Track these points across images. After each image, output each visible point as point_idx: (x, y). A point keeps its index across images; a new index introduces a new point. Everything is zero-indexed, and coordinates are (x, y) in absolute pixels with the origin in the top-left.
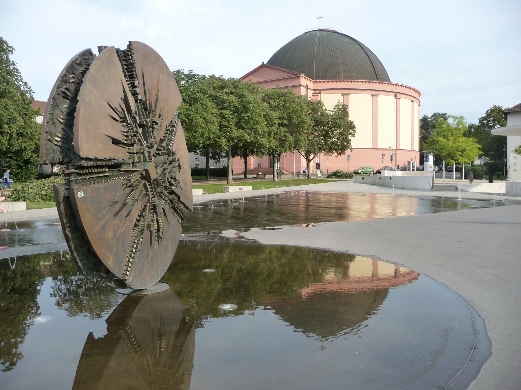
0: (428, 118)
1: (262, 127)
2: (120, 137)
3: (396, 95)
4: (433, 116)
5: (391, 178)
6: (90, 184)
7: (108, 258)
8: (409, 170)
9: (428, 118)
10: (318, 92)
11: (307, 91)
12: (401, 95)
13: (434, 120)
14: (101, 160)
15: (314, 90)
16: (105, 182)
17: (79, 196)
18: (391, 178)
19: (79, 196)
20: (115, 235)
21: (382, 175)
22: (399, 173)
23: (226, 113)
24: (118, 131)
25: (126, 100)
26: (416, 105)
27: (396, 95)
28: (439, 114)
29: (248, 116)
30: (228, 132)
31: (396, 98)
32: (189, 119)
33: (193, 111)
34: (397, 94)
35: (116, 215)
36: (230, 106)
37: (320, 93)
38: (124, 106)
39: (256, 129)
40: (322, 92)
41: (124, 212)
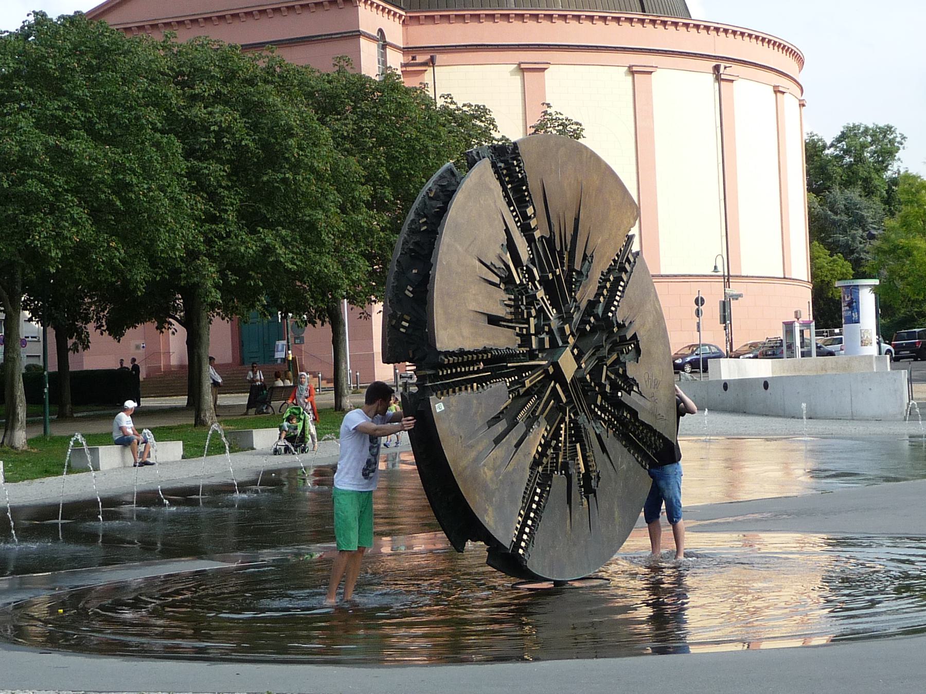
0: (824, 147)
1: (329, 219)
2: (501, 311)
3: (717, 68)
4: (843, 137)
5: (766, 385)
6: (454, 392)
7: (486, 511)
8: (792, 355)
9: (824, 147)
10: (424, 57)
11: (384, 55)
12: (736, 69)
13: (847, 152)
14: (469, 352)
15: (406, 50)
16: (478, 387)
17: (438, 411)
18: (766, 385)
19: (438, 411)
20: (497, 475)
21: (712, 375)
22: (763, 369)
23: (215, 170)
24: (497, 302)
25: (511, 246)
26: (790, 101)
27: (717, 68)
28: (867, 130)
29: (284, 181)
30: (221, 238)
31: (718, 78)
32: (126, 201)
33: (134, 172)
34: (723, 65)
35: (497, 441)
36: (219, 145)
37: (432, 62)
38: (508, 257)
39: (312, 226)
40: (439, 58)
41: (513, 437)
